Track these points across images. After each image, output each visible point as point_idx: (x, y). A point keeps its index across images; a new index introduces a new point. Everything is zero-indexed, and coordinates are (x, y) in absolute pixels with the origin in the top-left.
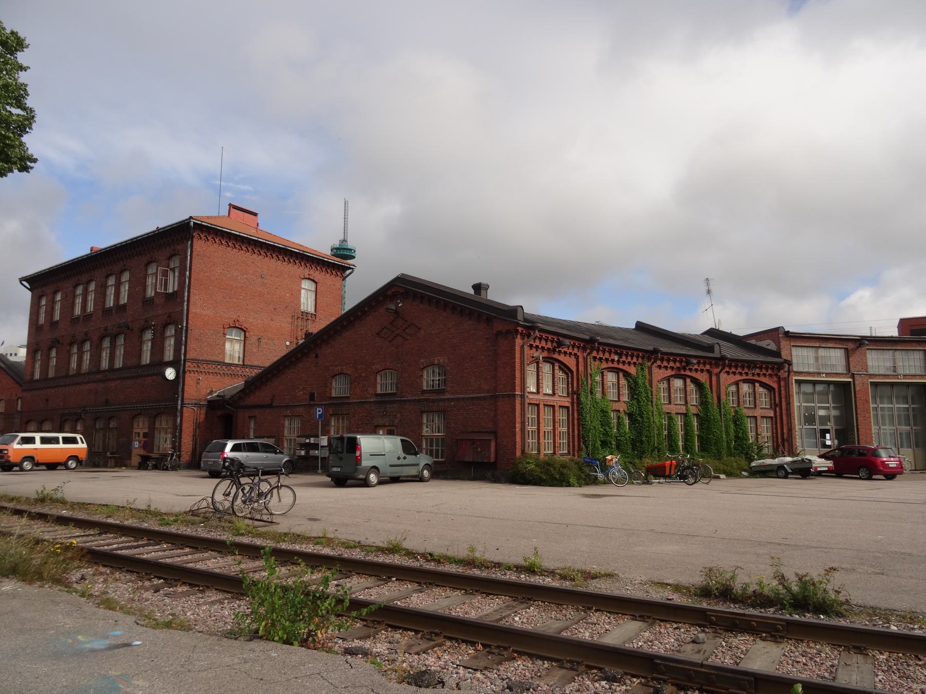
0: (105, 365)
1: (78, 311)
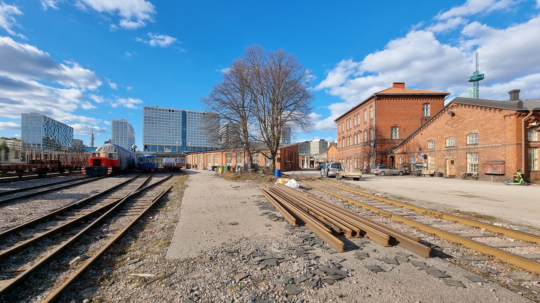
0: (355, 143)
1: (348, 128)
